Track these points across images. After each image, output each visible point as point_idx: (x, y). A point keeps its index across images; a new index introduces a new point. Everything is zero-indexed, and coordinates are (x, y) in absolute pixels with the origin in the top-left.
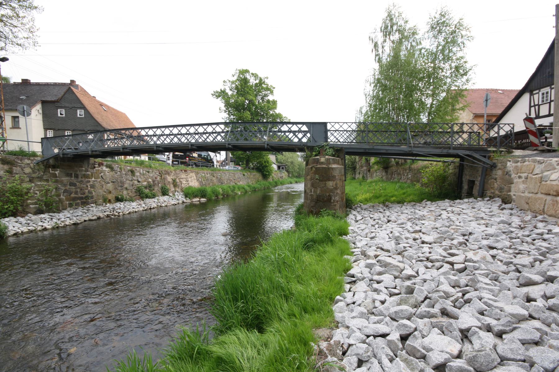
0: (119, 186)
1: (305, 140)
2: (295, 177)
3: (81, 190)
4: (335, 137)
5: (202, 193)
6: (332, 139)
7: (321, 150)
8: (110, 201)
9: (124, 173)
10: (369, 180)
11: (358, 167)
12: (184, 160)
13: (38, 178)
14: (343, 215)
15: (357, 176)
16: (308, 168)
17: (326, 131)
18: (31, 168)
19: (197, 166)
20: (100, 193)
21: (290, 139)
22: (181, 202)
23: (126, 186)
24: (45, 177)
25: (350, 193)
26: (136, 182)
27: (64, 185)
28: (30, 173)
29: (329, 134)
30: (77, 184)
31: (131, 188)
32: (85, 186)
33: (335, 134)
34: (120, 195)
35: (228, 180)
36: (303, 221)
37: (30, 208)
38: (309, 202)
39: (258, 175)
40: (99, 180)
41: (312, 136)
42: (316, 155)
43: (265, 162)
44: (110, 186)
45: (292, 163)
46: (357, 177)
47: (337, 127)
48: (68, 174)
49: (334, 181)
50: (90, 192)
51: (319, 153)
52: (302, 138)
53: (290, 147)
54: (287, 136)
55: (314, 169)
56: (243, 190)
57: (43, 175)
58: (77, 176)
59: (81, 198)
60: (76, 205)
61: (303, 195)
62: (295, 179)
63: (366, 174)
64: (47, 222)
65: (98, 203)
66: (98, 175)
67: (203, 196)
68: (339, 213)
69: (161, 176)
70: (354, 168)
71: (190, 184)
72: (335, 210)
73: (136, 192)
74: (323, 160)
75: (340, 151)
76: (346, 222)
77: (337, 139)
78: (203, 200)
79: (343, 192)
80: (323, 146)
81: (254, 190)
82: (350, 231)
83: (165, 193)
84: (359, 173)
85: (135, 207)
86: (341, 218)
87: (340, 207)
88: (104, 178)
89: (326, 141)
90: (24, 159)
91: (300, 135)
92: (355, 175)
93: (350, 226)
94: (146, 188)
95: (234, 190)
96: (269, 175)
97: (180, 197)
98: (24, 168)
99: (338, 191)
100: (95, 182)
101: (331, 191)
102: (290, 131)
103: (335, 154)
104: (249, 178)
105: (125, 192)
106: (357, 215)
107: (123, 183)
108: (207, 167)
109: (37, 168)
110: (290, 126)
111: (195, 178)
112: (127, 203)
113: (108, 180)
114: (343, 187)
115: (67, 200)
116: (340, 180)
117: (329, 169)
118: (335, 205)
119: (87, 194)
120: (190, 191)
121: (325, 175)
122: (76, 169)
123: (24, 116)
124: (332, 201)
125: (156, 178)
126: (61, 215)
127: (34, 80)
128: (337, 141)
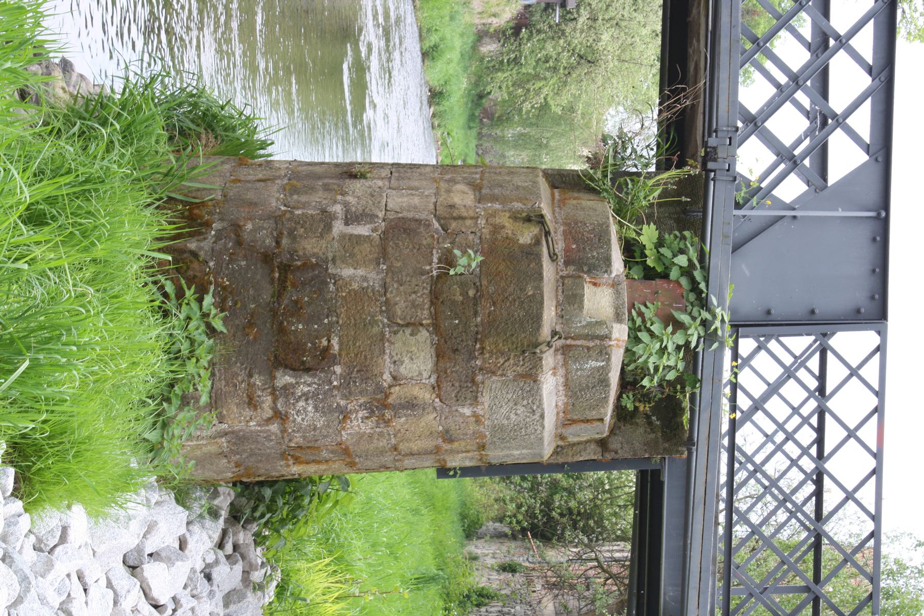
1: (751, 159)
2: (478, 81)
4: (773, 389)
6: (759, 366)
7: (670, 283)
11: (554, 555)
14: (179, 460)
15: (490, 552)
16: (533, 191)
17: (821, 323)
21: (760, 44)
25: (356, 505)
29: (799, 343)
33: (793, 392)
36: (118, 165)
38: (274, 199)
41: (786, 217)
42: (631, 250)
45: (588, 59)
46: (478, 548)
47: (850, 403)
49: (437, 387)
51: (650, 274)
52: (770, 141)
53: (700, 48)
54: (784, 22)
55: (526, 235)
61: (332, 153)
62: (459, 88)
68: (195, 435)
70: (542, 529)
72: (216, 401)
75: (661, 421)
76: (126, 482)
77: (758, 405)
79: (348, 456)
80: (704, 303)
82: (51, 519)
84: (510, 568)
86: (154, 449)
87: (239, 438)
89: (738, 327)
91: (789, 125)
92: (500, 536)
93: (94, 515)
99: (360, 424)
101: (362, 371)
102: (823, 43)
103: (645, 396)
106: (182, 570)
110: (865, 43)
114: (394, 459)
116: (447, 436)
117: (530, 350)
118: (252, 403)
121: (484, 318)
124: (284, 379)
128: (744, 402)
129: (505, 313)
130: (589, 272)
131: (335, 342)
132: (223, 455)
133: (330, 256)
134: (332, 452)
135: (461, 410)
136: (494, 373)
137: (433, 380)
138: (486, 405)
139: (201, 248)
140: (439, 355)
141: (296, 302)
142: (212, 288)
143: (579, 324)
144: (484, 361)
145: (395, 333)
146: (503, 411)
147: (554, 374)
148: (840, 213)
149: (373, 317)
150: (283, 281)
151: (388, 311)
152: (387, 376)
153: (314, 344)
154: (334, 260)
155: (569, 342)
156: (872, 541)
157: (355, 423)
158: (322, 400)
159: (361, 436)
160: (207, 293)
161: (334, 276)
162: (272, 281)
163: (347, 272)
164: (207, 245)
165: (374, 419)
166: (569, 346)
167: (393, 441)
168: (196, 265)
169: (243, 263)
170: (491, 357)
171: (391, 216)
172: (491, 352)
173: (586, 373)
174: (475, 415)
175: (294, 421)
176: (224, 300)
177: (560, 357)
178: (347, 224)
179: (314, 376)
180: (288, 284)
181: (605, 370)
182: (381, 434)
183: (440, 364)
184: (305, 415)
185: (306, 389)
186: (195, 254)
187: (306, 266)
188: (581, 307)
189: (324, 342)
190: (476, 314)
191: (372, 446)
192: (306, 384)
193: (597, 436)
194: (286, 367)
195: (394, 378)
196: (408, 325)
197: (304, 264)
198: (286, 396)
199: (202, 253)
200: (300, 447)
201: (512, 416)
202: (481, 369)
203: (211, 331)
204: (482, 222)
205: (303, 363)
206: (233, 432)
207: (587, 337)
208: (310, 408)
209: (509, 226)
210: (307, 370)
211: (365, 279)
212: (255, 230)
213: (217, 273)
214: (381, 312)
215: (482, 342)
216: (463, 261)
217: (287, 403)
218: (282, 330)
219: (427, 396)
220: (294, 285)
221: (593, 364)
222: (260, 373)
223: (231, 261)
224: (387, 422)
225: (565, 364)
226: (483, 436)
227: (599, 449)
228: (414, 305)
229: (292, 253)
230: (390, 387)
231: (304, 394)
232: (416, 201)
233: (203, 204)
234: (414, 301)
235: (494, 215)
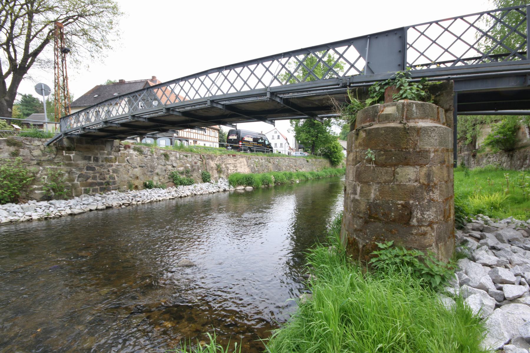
0: (148, 171)
3: (101, 174)
5: (248, 181)
8: (136, 188)
9: (156, 157)
10: (474, 169)
12: (237, 145)
13: (48, 160)
18: (41, 150)
19: (252, 151)
20: (124, 178)
22: (221, 190)
23: (157, 171)
24: (56, 161)
26: (170, 167)
27: (80, 169)
28: (39, 156)
30: (96, 168)
31: (164, 174)
32: (105, 170)
34: (149, 181)
35: (287, 166)
37: (35, 193)
39: (325, 162)
40: (124, 164)
43: (334, 147)
44: (138, 171)
48: (85, 157)
49: (421, 166)
50: (112, 177)
55: (363, 134)
56: (303, 178)
57: (54, 158)
58: (96, 160)
59: (101, 184)
60: (93, 191)
63: (468, 160)
64: (62, 208)
65: (121, 190)
66: (124, 159)
67: (249, 184)
69: (203, 161)
71: (238, 171)
72: (423, 248)
73: (169, 178)
74: (390, 110)
78: (249, 188)
81: (318, 178)
83: (205, 179)
85: (162, 195)
87: (439, 239)
88: (130, 162)
90: (34, 141)
94: (182, 173)
95: (291, 178)
96: (338, 162)
97: (223, 184)
98: (34, 149)
99: (436, 195)
100: (119, 167)
101: (413, 193)
104: (314, 164)
105: (156, 178)
107: (153, 168)
108: (263, 152)
109: (47, 149)
111: (246, 163)
112: (156, 190)
113: (135, 164)
114: (449, 182)
115: (82, 185)
116: (443, 162)
117: (406, 131)
118: (424, 234)
119: (107, 179)
120: (234, 179)
122: (96, 151)
123: (42, 95)
124: (414, 222)
125: (196, 163)
126: (72, 202)
127: (127, 80)
129: (391, 140)
130: (377, 113)
131: (400, 202)
132: (445, 244)
133: (366, 201)
134: (446, 204)
135: (432, 157)
136: (416, 144)
137: (418, 167)
138: (430, 147)
139: (362, 244)
140: (407, 164)
141: (383, 215)
142: (376, 243)
143: (397, 115)
144: (411, 148)
145: (397, 180)
146: (433, 141)
147: (418, 123)
148: (367, 49)
149: (390, 188)
150: (374, 218)
151: (388, 183)
152: (415, 184)
153: (400, 210)
154: (368, 200)
155: (404, 118)
156: (491, 13)
157: (435, 197)
158: (424, 208)
159: (440, 194)
160: (377, 245)
161: (374, 200)
162: (374, 222)
163: (372, 196)
164: (361, 241)
165: (434, 189)
166: (406, 117)
167: (443, 182)
168: (368, 246)
169: (368, 230)
170: (409, 145)
171: (355, 180)
172: (407, 145)
173: (418, 111)
174: (434, 152)
175: (433, 219)
176: (381, 239)
177: (411, 121)
178: (356, 194)
179: (414, 211)
180: (376, 216)
181: (417, 105)
182: (440, 187)
183: (411, 164)
184: (430, 215)
185: (419, 214)
186: (364, 246)
187: (370, 209)
188: (391, 114)
189: (400, 206)
190: (391, 151)
191: (445, 190)
192: (417, 214)
193: (444, 112)
194: (409, 221)
195: (416, 181)
196: (394, 175)
197: (369, 210)
198: (422, 221)
199: (364, 244)
200: (444, 216)
201: (435, 138)
202: (414, 149)
203: (393, 246)
204: (358, 150)
205: (408, 214)
206: (436, 241)
207: (403, 112)
208: (428, 213)
209: (360, 140)
210: (411, 213)
211: (375, 190)
212: (357, 225)
213: (371, 240)
214: (388, 185)
215: (402, 148)
216: (369, 155)
217: (425, 222)
218: (394, 221)
219: (425, 169)
220: (377, 215)
221: (414, 109)
222: (411, 231)
223: (367, 234)
224: (435, 184)
225: (414, 119)
226: (443, 150)
227: (449, 112)
228: (386, 173)
229: (365, 213)
230: (420, 183)
231: (421, 215)
232: (351, 171)
233: (348, 239)
234: (385, 173)
235: (356, 146)
